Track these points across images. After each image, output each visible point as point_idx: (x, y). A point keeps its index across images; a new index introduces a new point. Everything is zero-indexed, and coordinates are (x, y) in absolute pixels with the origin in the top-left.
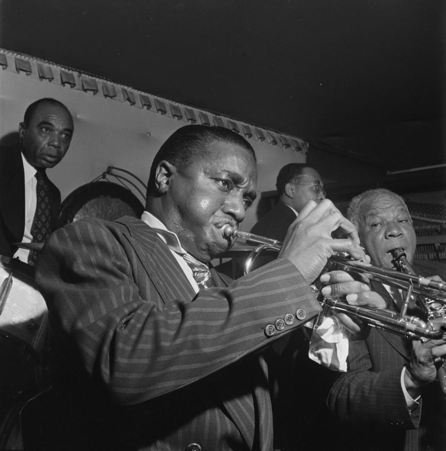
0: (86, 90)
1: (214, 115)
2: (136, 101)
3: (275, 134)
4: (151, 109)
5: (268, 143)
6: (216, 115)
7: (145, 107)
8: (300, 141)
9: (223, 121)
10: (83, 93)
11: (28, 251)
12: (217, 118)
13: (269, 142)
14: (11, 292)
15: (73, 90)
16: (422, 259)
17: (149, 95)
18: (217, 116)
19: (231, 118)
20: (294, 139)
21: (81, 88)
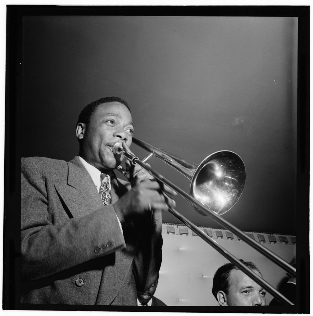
0: (181, 234)
1: (269, 235)
2: (223, 236)
4: (223, 238)
6: (270, 234)
7: (220, 238)
9: (275, 237)
10: (181, 235)
11: (272, 297)
12: (271, 236)
15: (174, 235)
18: (271, 235)
19: (281, 235)
21: (179, 234)
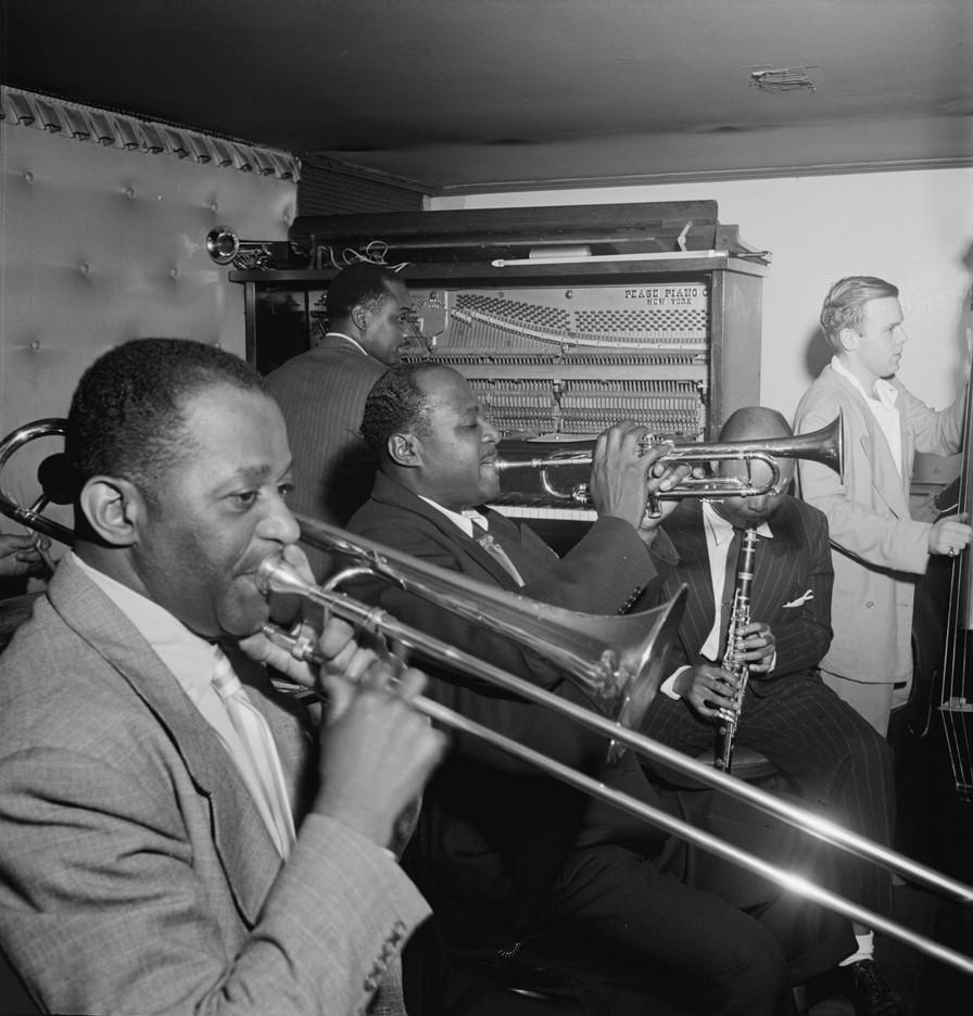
1: (141, 122)
3: (245, 148)
5: (275, 178)
8: (287, 157)
13: (16, 120)
14: (594, 289)
16: (513, 396)
17: (25, 92)
18: (147, 123)
20: (276, 153)
